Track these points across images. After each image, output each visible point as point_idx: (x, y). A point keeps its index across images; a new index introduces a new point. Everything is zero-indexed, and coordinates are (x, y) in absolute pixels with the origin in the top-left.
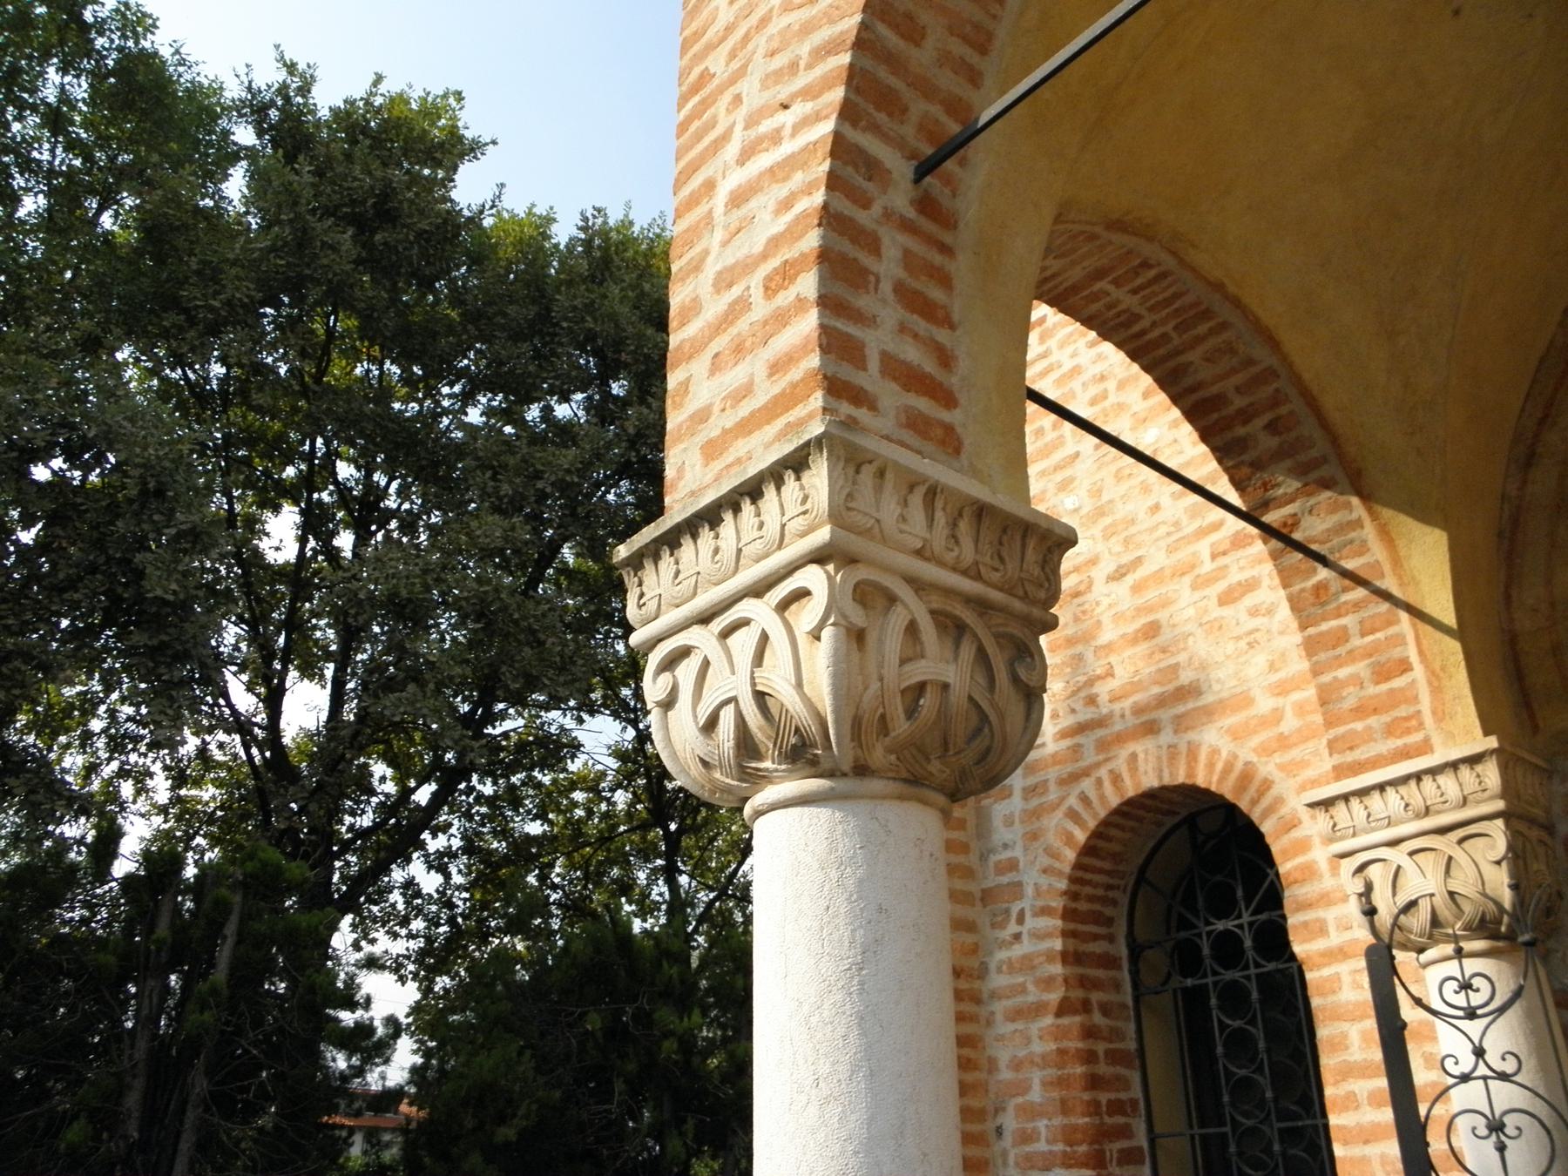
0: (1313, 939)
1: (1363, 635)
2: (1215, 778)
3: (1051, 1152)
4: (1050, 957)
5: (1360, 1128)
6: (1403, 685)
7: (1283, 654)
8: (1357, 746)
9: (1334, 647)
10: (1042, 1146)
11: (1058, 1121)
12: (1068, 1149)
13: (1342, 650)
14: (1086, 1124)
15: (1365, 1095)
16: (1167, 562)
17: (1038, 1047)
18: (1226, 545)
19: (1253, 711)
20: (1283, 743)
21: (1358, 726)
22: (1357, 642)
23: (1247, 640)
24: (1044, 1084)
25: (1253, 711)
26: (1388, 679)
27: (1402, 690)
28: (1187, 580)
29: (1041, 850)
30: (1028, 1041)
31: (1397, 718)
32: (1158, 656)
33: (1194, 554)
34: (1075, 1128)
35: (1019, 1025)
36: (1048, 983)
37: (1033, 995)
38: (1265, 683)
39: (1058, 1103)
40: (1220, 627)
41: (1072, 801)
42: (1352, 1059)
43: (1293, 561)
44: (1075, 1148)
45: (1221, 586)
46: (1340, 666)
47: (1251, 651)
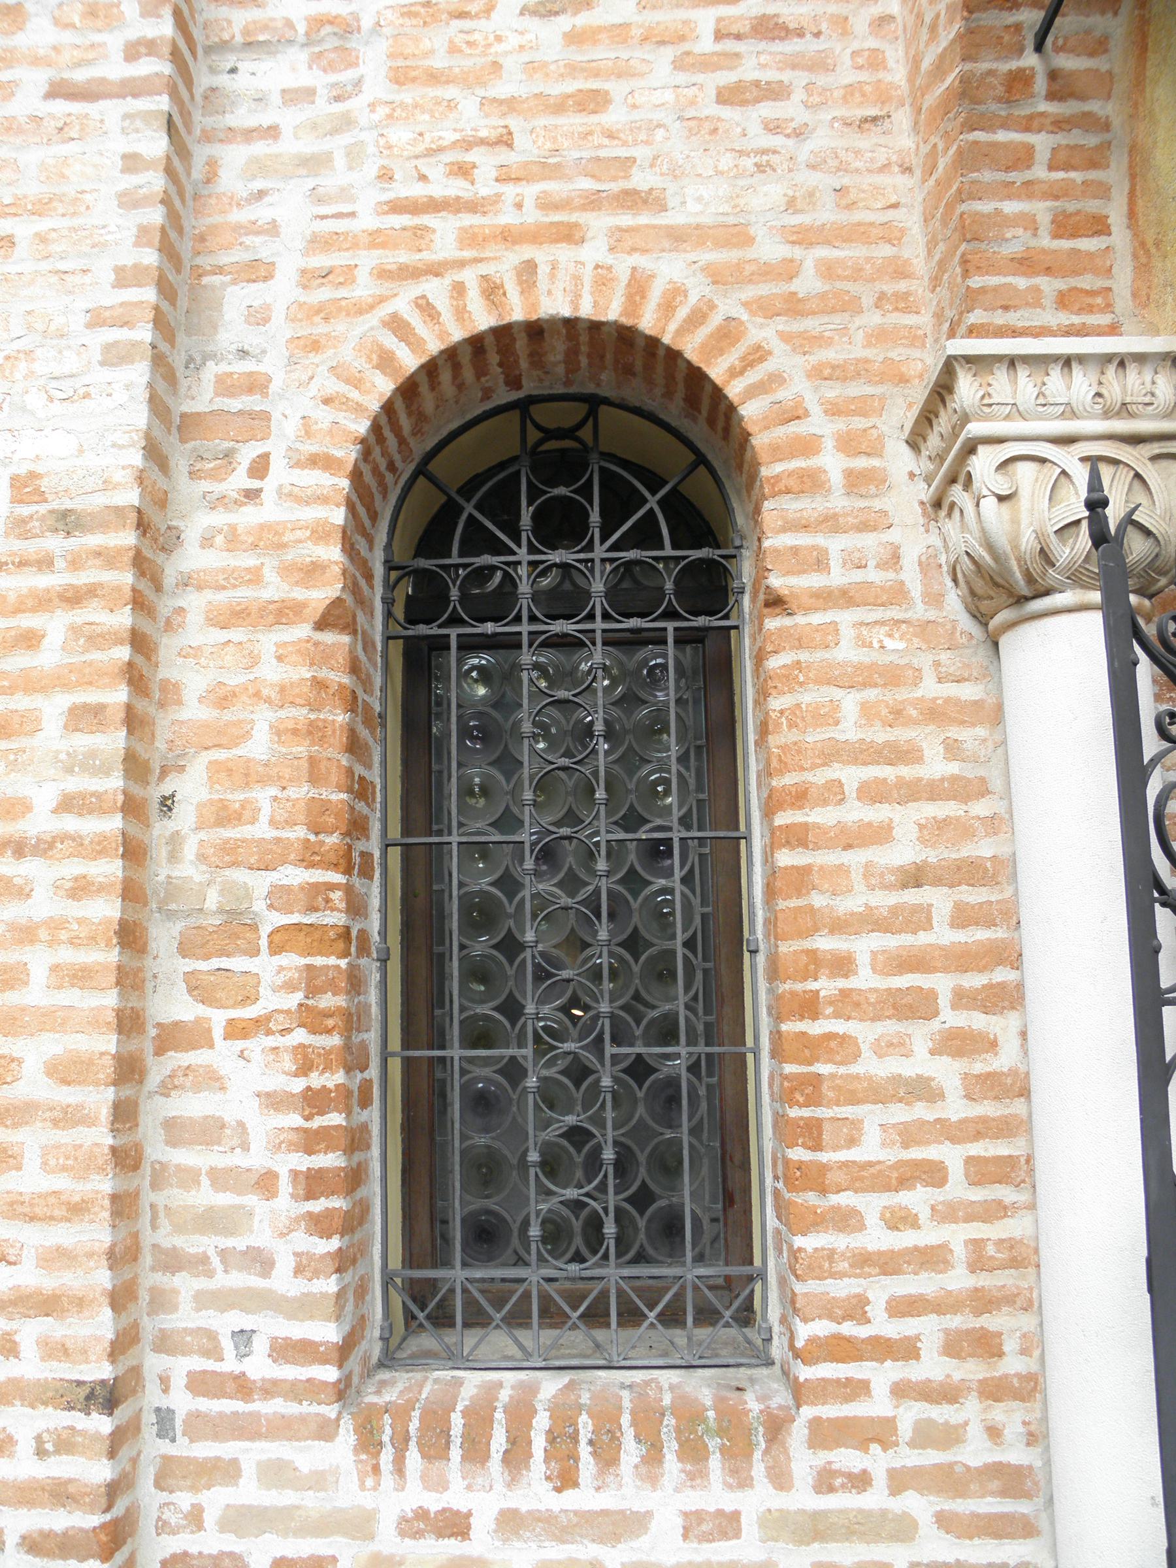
0: (804, 572)
1: (1051, 168)
2: (672, 327)
3: (278, 840)
4: (319, 533)
5: (842, 828)
6: (1093, 249)
7: (811, 194)
8: (1016, 308)
9: (1008, 169)
10: (262, 830)
11: (301, 792)
12: (312, 838)
13: (1017, 177)
14: (342, 801)
15: (856, 785)
16: (637, 19)
17: (271, 673)
18: (744, 27)
19: (751, 253)
20: (794, 306)
21: (1021, 283)
22: (1039, 172)
23: (757, 159)
24: (278, 732)
25: (751, 253)
26: (1074, 236)
27: (1090, 255)
28: (668, 53)
29: (323, 369)
30: (254, 661)
31: (1076, 288)
32: (597, 139)
33: (685, 22)
34: (324, 806)
35: (237, 634)
36: (312, 572)
37: (274, 588)
38: (779, 224)
39: (305, 764)
40: (715, 131)
41: (469, 277)
42: (842, 737)
43: (997, 23)
44: (321, 837)
45: (726, 78)
46: (1009, 197)
47: (759, 177)
